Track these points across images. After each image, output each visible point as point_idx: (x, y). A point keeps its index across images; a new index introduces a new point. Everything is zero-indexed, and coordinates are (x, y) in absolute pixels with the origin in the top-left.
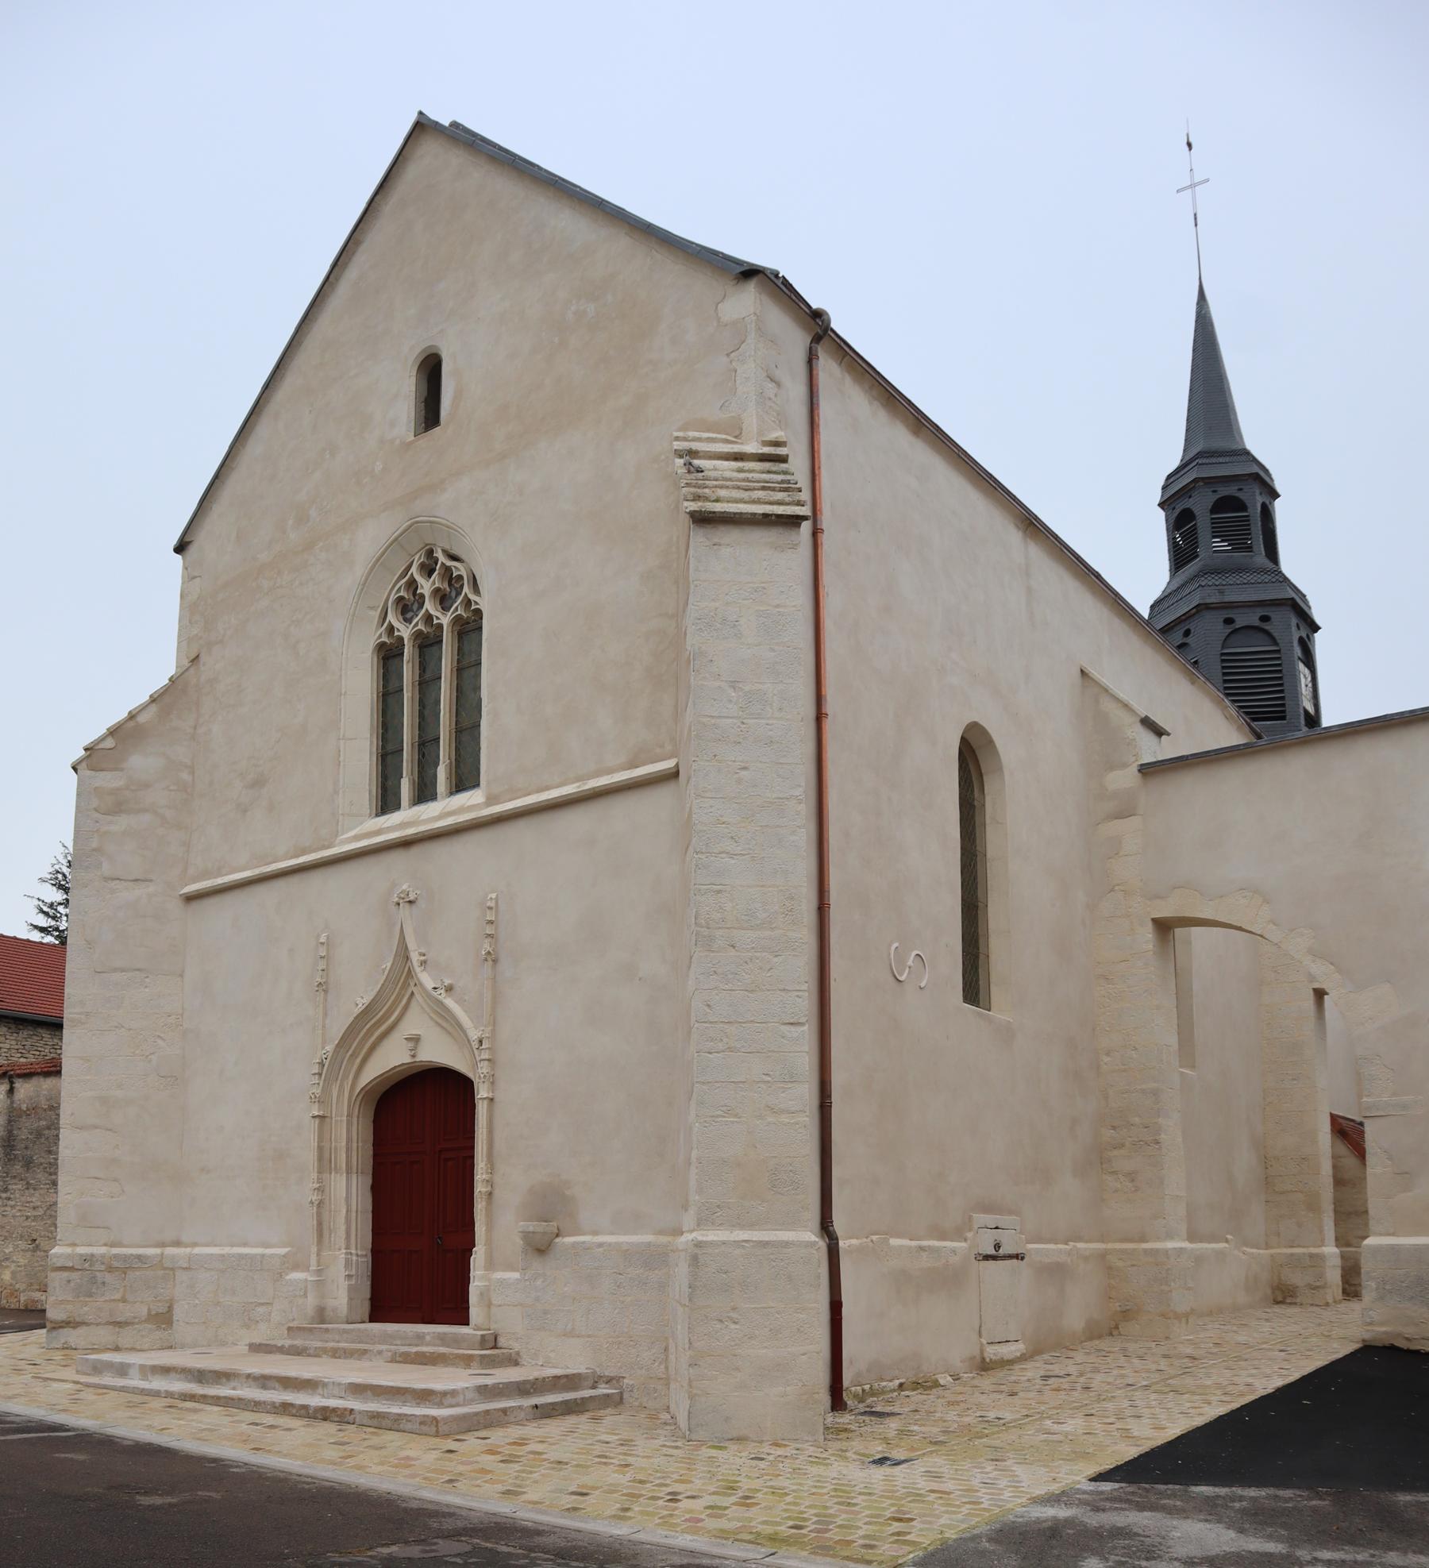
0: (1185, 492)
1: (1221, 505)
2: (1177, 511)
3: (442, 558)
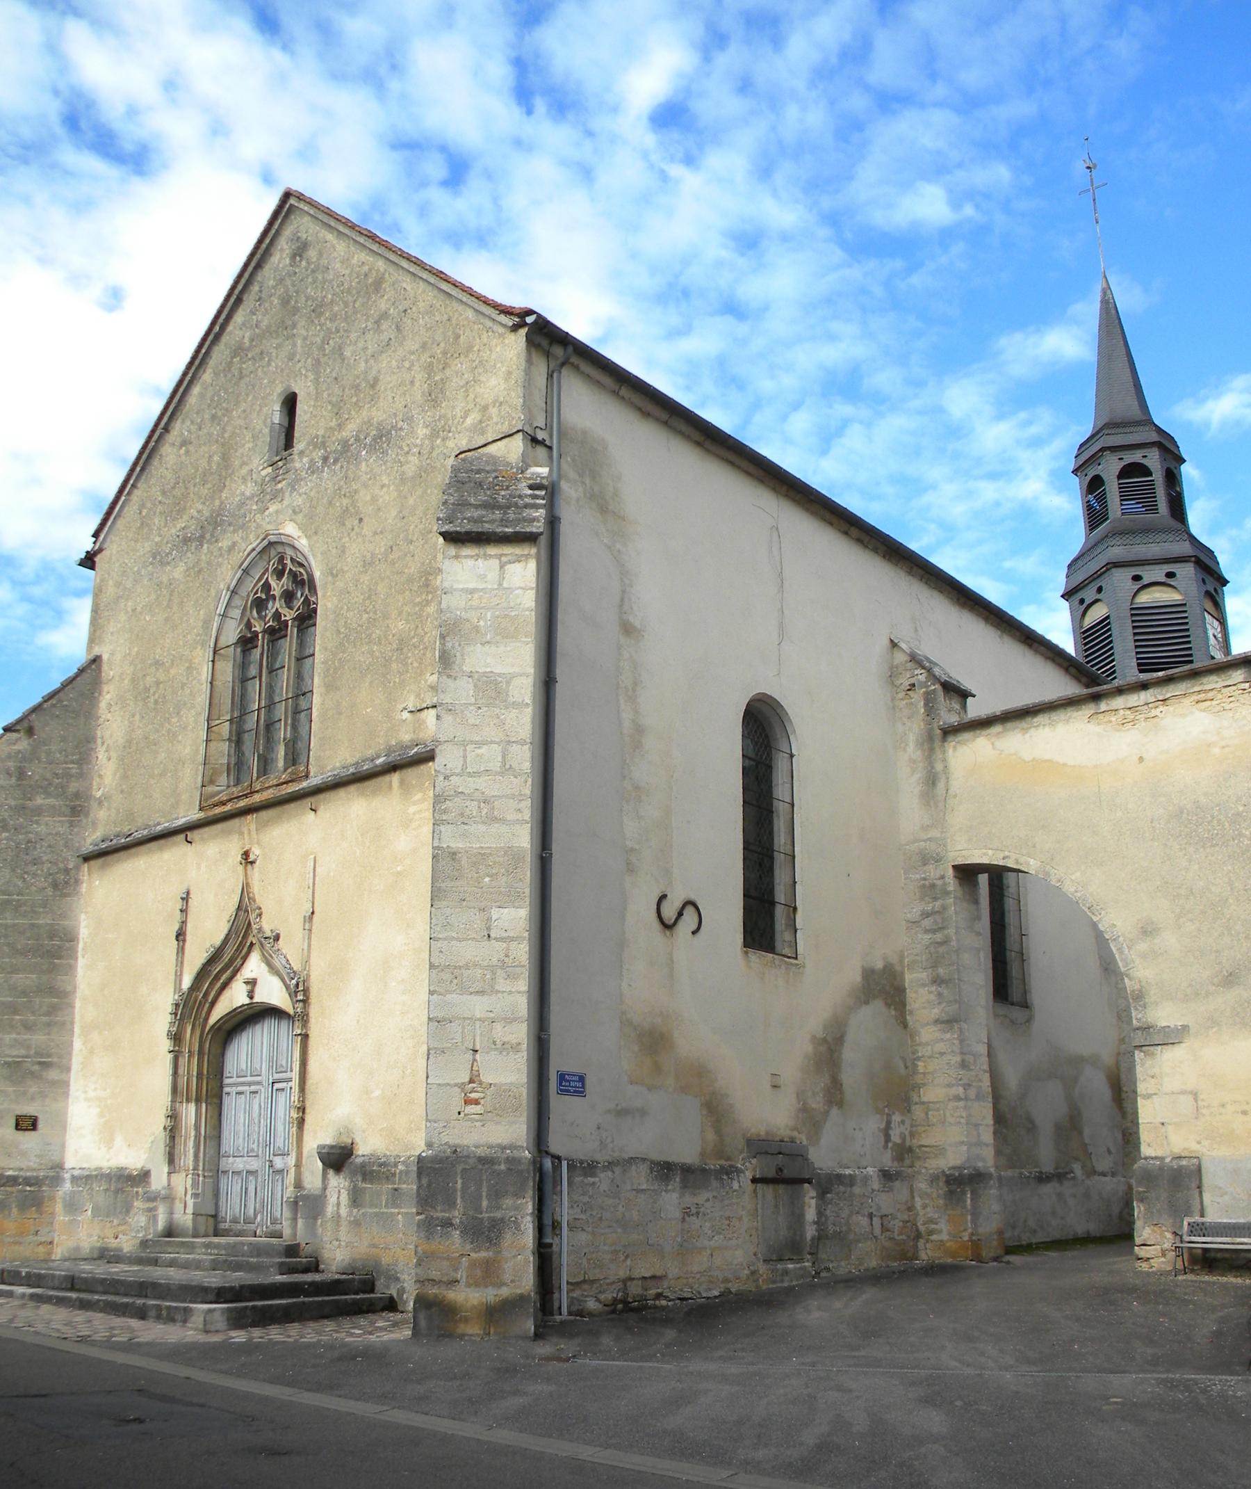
0: (1094, 459)
1: (1130, 470)
2: (1089, 478)
3: (289, 565)
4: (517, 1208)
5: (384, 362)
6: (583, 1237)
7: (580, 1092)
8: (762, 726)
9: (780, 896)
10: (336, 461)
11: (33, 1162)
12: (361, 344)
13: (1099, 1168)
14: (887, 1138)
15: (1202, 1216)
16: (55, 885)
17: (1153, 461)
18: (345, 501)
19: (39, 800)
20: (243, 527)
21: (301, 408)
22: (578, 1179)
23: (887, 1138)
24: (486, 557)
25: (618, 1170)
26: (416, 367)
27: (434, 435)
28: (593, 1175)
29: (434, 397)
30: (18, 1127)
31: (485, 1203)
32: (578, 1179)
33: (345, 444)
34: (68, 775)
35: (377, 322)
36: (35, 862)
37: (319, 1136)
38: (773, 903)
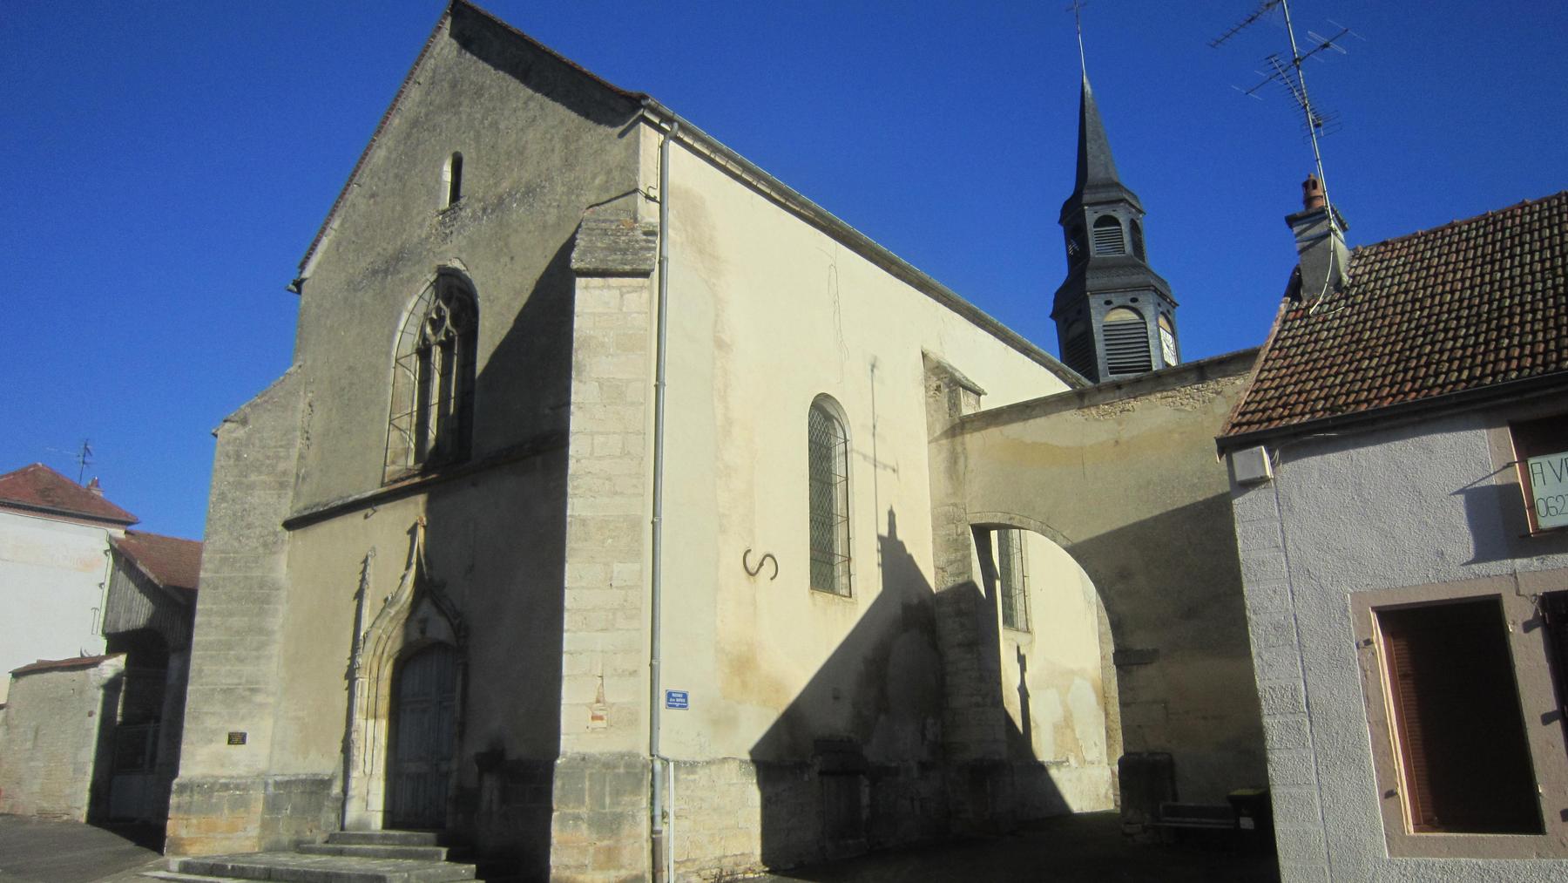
4: (633, 804)
5: (530, 135)
6: (686, 823)
7: (684, 706)
8: (824, 414)
9: (839, 549)
10: (493, 211)
11: (241, 770)
12: (513, 120)
13: (1088, 758)
14: (924, 736)
15: (1175, 800)
16: (265, 545)
17: (1122, 216)
18: (501, 244)
19: (253, 477)
20: (419, 262)
21: (465, 169)
22: (682, 776)
23: (924, 736)
24: (609, 287)
25: (714, 768)
26: (556, 139)
27: (570, 192)
28: (693, 772)
29: (568, 164)
30: (230, 742)
31: (608, 801)
32: (682, 776)
33: (501, 200)
34: (278, 458)
35: (525, 103)
36: (249, 526)
37: (476, 746)
38: (832, 554)
